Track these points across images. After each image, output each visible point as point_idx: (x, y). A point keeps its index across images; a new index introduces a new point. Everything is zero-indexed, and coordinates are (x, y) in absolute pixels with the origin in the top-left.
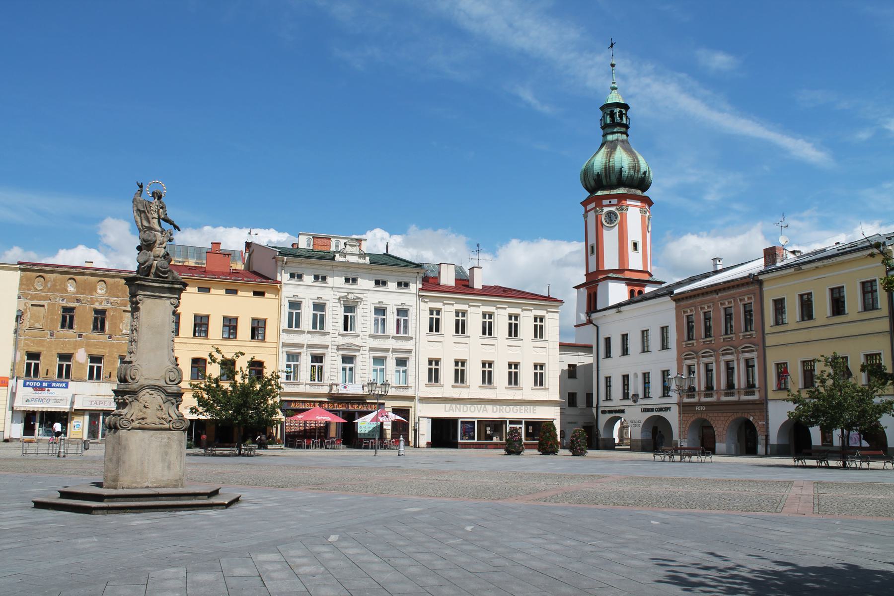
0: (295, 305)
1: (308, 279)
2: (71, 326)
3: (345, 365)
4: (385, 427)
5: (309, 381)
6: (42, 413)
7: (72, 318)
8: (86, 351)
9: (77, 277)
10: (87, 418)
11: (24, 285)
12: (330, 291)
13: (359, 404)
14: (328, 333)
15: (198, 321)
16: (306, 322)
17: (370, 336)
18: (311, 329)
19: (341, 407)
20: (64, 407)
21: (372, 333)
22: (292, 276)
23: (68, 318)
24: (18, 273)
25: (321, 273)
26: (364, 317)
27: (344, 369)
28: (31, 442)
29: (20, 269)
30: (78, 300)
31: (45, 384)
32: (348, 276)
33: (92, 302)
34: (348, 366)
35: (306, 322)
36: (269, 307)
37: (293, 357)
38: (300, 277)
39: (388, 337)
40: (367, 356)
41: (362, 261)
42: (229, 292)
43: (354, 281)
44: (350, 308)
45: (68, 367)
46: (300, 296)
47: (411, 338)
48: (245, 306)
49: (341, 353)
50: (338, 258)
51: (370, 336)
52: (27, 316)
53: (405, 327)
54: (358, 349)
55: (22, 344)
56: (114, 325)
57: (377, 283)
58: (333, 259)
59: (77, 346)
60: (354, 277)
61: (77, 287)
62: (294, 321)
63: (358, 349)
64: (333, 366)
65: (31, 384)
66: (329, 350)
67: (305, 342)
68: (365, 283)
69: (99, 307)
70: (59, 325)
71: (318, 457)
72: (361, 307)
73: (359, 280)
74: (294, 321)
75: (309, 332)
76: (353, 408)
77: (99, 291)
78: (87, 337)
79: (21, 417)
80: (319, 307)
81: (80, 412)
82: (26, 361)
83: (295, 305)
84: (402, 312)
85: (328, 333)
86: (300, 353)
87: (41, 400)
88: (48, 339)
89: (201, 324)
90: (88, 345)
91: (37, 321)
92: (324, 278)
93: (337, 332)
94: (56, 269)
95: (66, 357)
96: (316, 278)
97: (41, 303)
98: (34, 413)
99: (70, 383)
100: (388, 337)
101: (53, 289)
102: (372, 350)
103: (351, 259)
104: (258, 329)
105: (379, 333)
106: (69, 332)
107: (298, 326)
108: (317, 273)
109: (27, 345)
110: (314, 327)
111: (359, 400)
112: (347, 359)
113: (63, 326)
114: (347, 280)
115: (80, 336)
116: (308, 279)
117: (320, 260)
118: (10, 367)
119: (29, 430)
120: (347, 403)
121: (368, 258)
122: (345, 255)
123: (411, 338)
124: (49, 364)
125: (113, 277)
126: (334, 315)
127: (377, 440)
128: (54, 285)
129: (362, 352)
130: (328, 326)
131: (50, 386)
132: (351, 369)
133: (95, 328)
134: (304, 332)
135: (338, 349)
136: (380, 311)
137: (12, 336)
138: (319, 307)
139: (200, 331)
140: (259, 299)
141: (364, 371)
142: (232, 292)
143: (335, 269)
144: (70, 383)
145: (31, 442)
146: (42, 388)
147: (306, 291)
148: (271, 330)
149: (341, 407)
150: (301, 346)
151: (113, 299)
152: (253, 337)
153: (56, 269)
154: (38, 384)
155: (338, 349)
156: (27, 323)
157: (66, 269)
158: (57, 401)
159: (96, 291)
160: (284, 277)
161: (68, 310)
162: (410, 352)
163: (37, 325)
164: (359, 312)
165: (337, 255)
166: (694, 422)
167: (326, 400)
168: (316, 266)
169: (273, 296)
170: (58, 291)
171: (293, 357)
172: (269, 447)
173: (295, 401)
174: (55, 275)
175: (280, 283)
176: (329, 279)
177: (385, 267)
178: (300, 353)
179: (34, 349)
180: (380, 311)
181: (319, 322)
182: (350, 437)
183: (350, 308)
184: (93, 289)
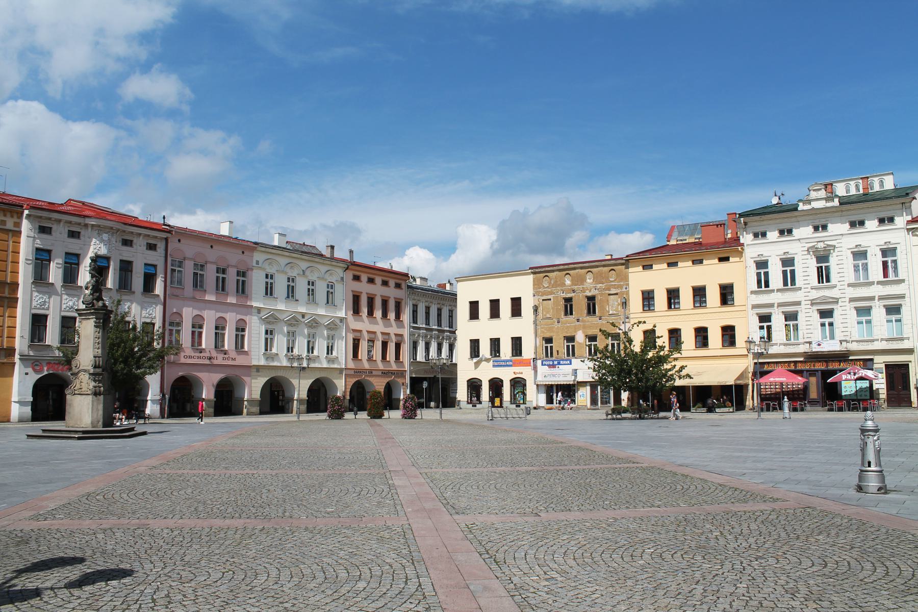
0: (762, 264)
1: (773, 235)
2: (571, 314)
3: (823, 320)
4: (875, 387)
5: (785, 341)
6: (557, 385)
7: (571, 306)
8: (584, 332)
9: (550, 274)
10: (588, 388)
11: (537, 284)
12: (797, 244)
13: (840, 361)
14: (800, 289)
15: (646, 295)
16: (776, 280)
17: (849, 285)
18: (881, 278)
19: (820, 366)
20: (569, 380)
21: (852, 281)
22: (756, 235)
23: (569, 306)
24: (531, 278)
25: (786, 226)
26: (841, 266)
27: (823, 325)
28: (551, 409)
29: (534, 273)
30: (574, 291)
31: (556, 363)
32: (817, 224)
33: (583, 291)
34: (827, 321)
35: (776, 280)
36: (739, 272)
37: (765, 318)
38: (764, 235)
39: (872, 283)
40: (848, 308)
41: (830, 204)
42: (645, 267)
43: (825, 227)
44: (822, 257)
45: (573, 346)
46: (765, 254)
47: (903, 281)
48: (712, 274)
49: (816, 307)
50: (801, 207)
51: (849, 285)
52: (540, 310)
53: (895, 268)
54: (836, 301)
55: (539, 331)
56: (603, 308)
57: (853, 225)
58: (796, 209)
59: (576, 329)
60: (823, 223)
61: (572, 281)
62: (763, 282)
63: (836, 301)
64: (809, 320)
65: (547, 363)
66: (803, 306)
67: (776, 302)
68: (838, 228)
69: (589, 294)
70: (563, 313)
71: (270, 422)
72: (834, 254)
73: (830, 226)
74: (763, 282)
75: (879, 283)
76: (833, 366)
77: (588, 281)
78: (583, 321)
79: (543, 389)
80: (788, 262)
81: (583, 384)
82: (566, 344)
83: (762, 264)
84: (888, 252)
85: (800, 289)
86: (871, 307)
87: (554, 376)
88: (556, 325)
89: (648, 298)
90: (584, 327)
91: (548, 312)
92: (790, 232)
93: (809, 286)
94: (555, 268)
95: (571, 339)
96: (782, 232)
97: (549, 297)
98: (552, 385)
99: (574, 360)
100: (872, 283)
101: (556, 285)
102: (852, 300)
103: (815, 205)
104: (726, 294)
105: (862, 281)
106: (570, 318)
107: (767, 285)
108: (782, 228)
109: (543, 332)
110: (785, 284)
111: (842, 357)
112: (826, 314)
113: (566, 314)
114: (816, 229)
115: (578, 321)
116: (773, 235)
117: (780, 215)
118: (533, 351)
119: (550, 400)
120: (826, 362)
121: (836, 200)
122: (809, 202)
123: (903, 281)
124: (559, 345)
125: (597, 267)
126: (806, 268)
127: (864, 400)
128: (556, 282)
129: (840, 304)
130: (799, 282)
131: (559, 364)
132: (831, 324)
133: (589, 313)
134: (773, 291)
135: (812, 304)
136: (860, 254)
137: (532, 326)
138: (788, 262)
139: (675, 303)
140: (724, 265)
141: (845, 325)
142: (672, 264)
143: (799, 219)
144: (574, 360)
145: (551, 409)
146: (553, 366)
147: (772, 247)
148: (738, 295)
149: (820, 366)
150: (771, 305)
151: (599, 286)
152: (670, 307)
153: (555, 268)
154: (551, 363)
155: (812, 304)
156: (540, 316)
157: (562, 267)
158: (565, 375)
159: (585, 281)
160: (747, 238)
161: (568, 300)
162: (902, 297)
163: (548, 316)
164: (833, 262)
165: (801, 204)
166: (502, 381)
167: (802, 359)
168: (778, 221)
169: (737, 259)
170: (559, 286)
171: (765, 318)
172: (717, 410)
173: (768, 363)
174: (555, 273)
175: (743, 245)
176: (795, 231)
177: (763, 217)
178: (871, 307)
179: (547, 335)
180: (860, 254)
181: (789, 279)
182: (831, 395)
183: (822, 257)
184: (582, 280)
